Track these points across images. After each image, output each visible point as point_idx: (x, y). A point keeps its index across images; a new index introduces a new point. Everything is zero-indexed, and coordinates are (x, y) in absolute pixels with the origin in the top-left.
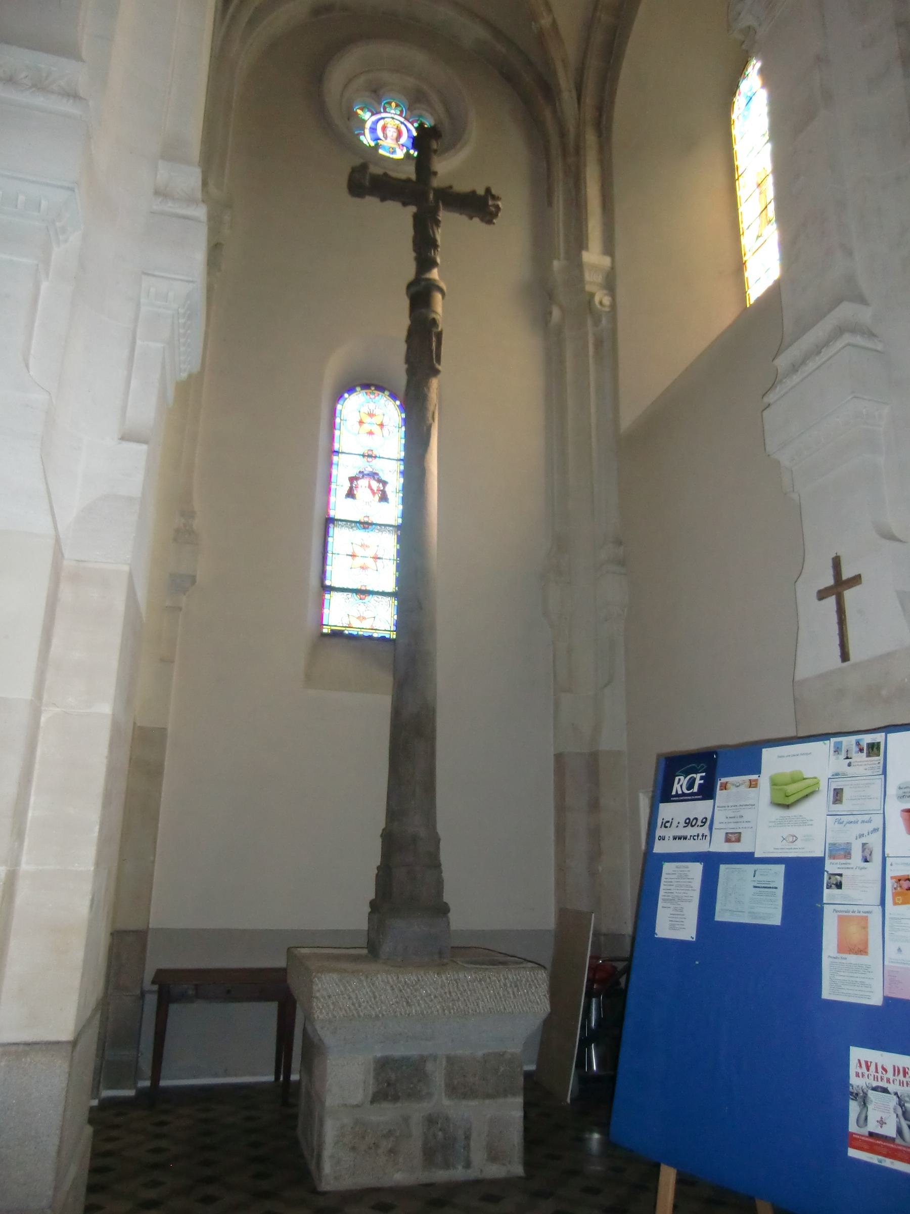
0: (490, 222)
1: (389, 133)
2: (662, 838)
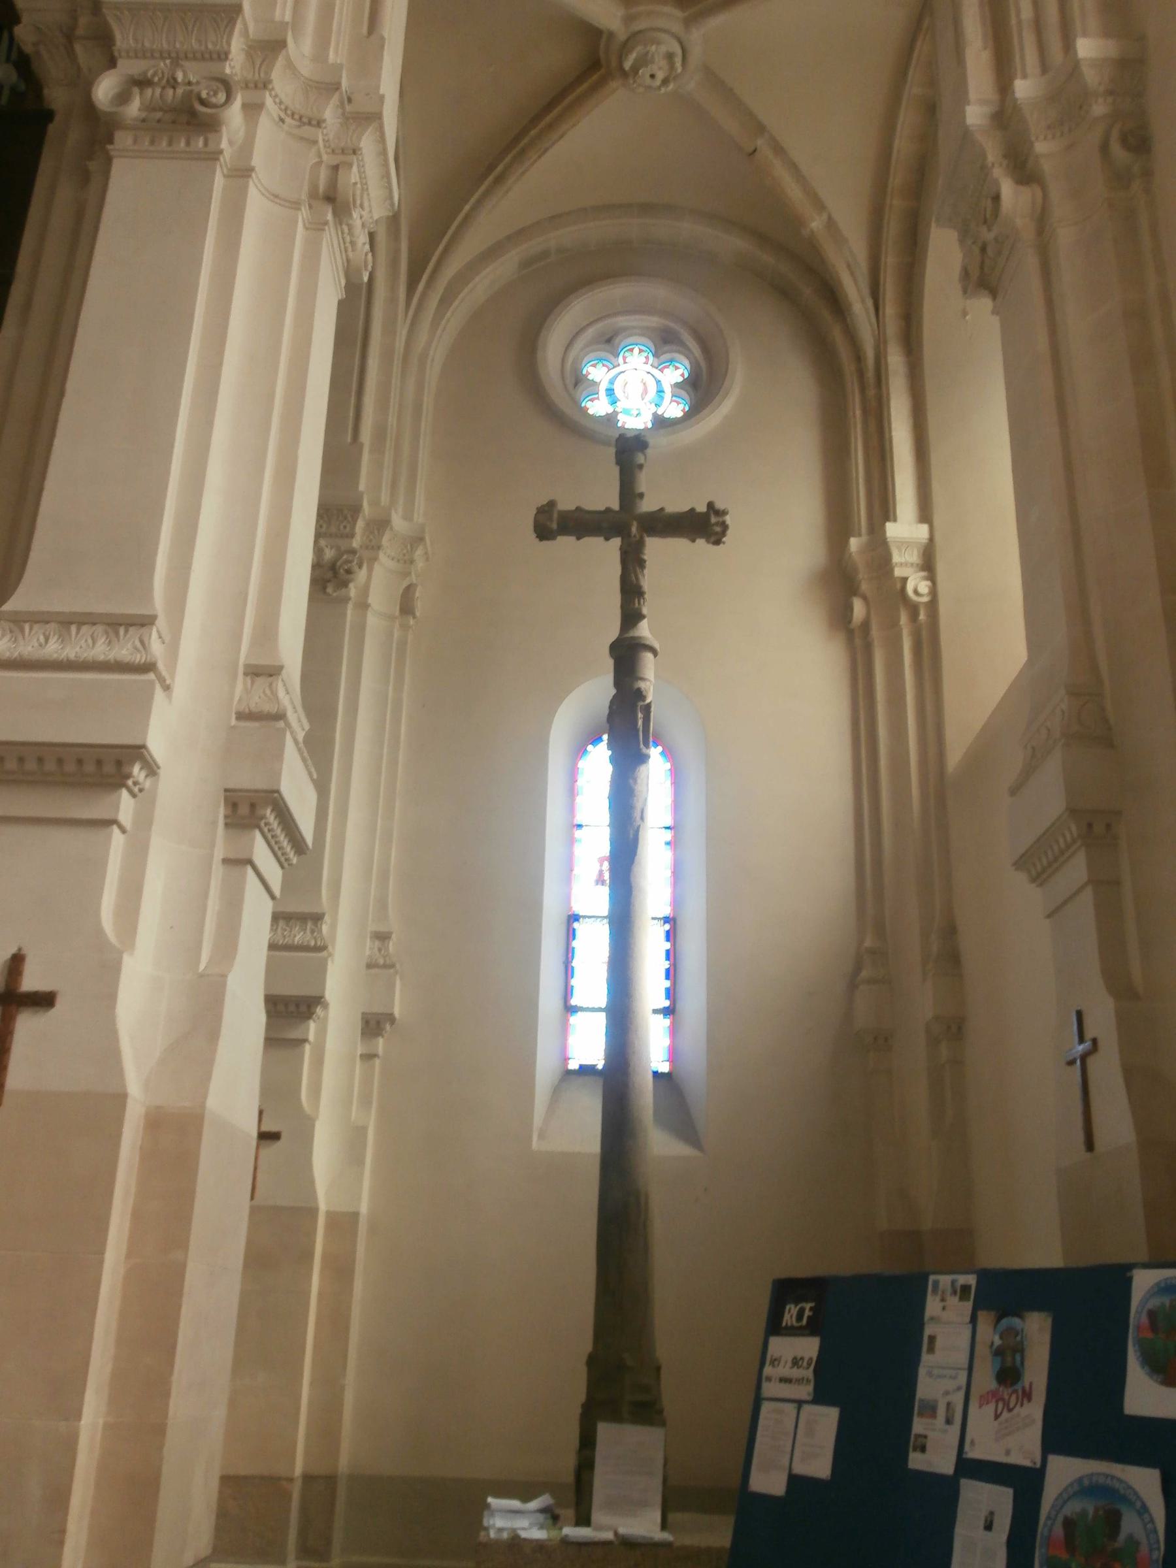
0: (718, 542)
1: (634, 388)
2: (769, 1379)
